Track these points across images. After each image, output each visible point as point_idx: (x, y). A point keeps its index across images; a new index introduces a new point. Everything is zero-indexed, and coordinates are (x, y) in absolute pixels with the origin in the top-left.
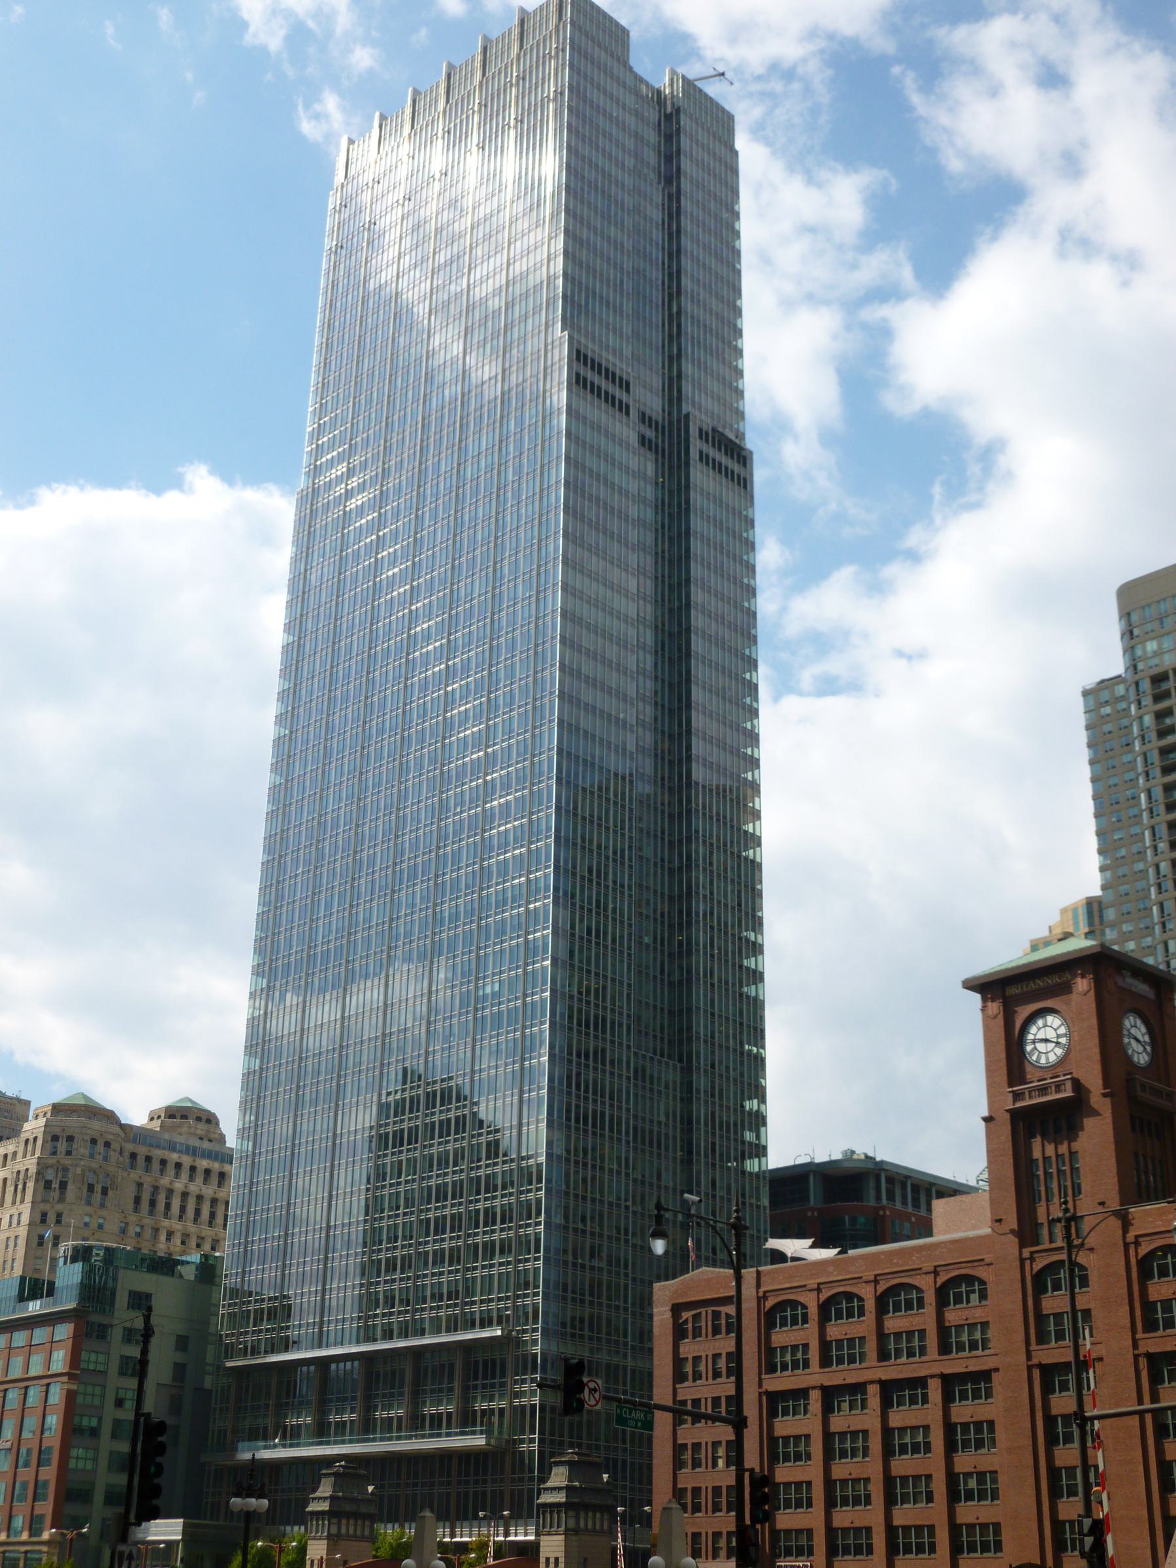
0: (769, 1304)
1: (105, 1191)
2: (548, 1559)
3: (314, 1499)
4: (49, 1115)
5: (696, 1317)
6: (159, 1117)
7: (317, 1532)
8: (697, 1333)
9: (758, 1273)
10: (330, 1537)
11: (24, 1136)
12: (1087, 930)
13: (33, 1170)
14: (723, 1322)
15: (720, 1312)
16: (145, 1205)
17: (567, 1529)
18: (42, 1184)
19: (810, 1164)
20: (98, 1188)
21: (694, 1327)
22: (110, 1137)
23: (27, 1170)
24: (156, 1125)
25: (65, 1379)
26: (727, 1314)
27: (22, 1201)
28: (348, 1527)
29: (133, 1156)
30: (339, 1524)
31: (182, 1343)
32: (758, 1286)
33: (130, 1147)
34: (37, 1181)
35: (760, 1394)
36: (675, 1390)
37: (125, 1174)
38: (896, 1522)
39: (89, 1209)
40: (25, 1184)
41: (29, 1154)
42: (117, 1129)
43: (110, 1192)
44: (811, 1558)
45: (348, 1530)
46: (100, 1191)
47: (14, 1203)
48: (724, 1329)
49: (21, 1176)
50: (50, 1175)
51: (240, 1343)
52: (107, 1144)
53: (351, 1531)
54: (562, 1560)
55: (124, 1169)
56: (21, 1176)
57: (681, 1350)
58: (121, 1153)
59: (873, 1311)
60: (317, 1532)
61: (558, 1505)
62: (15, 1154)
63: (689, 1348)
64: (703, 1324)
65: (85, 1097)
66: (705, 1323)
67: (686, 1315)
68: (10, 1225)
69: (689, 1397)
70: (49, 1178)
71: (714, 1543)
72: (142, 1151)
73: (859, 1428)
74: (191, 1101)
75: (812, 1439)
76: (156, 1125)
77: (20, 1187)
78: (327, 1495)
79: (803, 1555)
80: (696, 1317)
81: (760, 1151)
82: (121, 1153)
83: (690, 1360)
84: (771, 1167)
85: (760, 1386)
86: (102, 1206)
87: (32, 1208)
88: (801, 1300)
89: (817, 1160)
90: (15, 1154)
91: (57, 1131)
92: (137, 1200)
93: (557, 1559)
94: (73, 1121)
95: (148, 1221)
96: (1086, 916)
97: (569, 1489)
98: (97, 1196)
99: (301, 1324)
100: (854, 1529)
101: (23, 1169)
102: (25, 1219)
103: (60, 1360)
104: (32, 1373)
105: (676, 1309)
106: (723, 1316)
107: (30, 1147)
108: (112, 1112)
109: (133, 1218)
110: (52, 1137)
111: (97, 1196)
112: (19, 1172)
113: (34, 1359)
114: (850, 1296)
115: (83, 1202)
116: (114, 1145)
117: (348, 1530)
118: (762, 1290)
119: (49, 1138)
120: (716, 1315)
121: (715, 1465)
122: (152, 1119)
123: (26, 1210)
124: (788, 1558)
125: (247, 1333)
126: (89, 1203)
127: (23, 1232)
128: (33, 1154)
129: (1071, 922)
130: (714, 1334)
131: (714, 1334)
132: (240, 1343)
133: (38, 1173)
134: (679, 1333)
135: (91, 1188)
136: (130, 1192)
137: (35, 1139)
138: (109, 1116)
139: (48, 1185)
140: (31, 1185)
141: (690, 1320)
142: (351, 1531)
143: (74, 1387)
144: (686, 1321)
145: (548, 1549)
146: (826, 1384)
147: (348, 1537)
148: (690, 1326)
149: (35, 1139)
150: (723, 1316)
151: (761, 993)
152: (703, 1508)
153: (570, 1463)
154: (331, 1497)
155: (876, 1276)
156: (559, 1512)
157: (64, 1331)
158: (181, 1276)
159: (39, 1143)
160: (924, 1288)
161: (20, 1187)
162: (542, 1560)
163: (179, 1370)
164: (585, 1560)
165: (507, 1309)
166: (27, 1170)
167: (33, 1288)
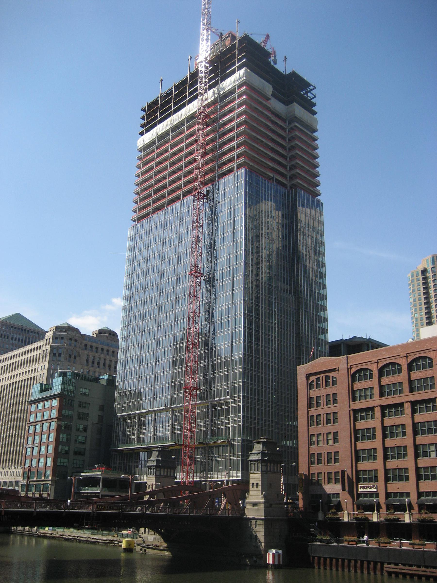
0: (353, 370)
1: (75, 357)
2: (253, 484)
3: (150, 460)
4: (54, 330)
5: (318, 379)
6: (96, 333)
7: (151, 474)
8: (318, 386)
9: (347, 357)
10: (156, 476)
11: (46, 338)
12: (432, 266)
13: (49, 350)
14: (331, 380)
15: (329, 376)
16: (90, 363)
17: (262, 471)
18: (52, 354)
19: (342, 340)
20: (73, 356)
21: (316, 384)
22: (77, 338)
23: (47, 350)
24: (95, 336)
25: (56, 420)
26: (332, 377)
27: (45, 361)
28: (164, 472)
29: (86, 345)
30: (160, 471)
31: (102, 408)
32: (347, 363)
33: (84, 342)
34: (50, 353)
35: (350, 410)
36: (308, 411)
37: (83, 351)
38: (419, 465)
39: (69, 364)
40: (46, 355)
41: (47, 344)
42: (79, 335)
43: (77, 358)
44: (376, 483)
45: (164, 473)
46: (73, 357)
47: (42, 361)
48: (331, 383)
49: (45, 352)
50: (55, 351)
51: (123, 407)
52: (76, 341)
53: (165, 474)
54: (260, 484)
55: (83, 350)
56: (45, 352)
57: (311, 394)
58: (81, 344)
59: (406, 370)
60: (151, 474)
61: (258, 460)
62: (43, 345)
63: (314, 393)
64: (321, 382)
65: (68, 324)
66: (323, 382)
67: (312, 378)
68: (41, 370)
69: (315, 414)
70: (54, 352)
71: (328, 477)
72: (89, 344)
73: (400, 423)
74: (107, 328)
75: (377, 429)
76: (95, 336)
77: (45, 356)
78: (155, 459)
79: (372, 481)
80: (318, 379)
81: (325, 331)
82: (81, 344)
83: (315, 398)
84: (330, 341)
85: (350, 408)
86: (74, 363)
87: (49, 363)
88: (369, 368)
89: (344, 339)
90: (43, 345)
91: (58, 336)
92: (87, 361)
93: (257, 484)
94: (64, 333)
95: (91, 368)
96: (432, 262)
97: (263, 454)
98: (73, 359)
99: (146, 401)
100: (398, 469)
101: (45, 349)
102: (46, 367)
103: (54, 413)
104: (45, 418)
105: (308, 376)
106: (331, 378)
107: (48, 342)
108: (78, 329)
109: (86, 367)
110: (56, 337)
111: (73, 359)
112: (44, 351)
113: (45, 413)
114: (393, 364)
115: (67, 361)
116: (79, 341)
117: (164, 473)
118: (349, 365)
119: (55, 338)
120: (327, 378)
121: (328, 443)
122: (93, 334)
123: (46, 363)
124: (364, 483)
125: (125, 403)
126: (70, 362)
127: (45, 371)
128: (49, 344)
129: (426, 264)
130: (326, 386)
131: (326, 386)
132: (123, 407)
133: (51, 351)
134: (310, 386)
135: (70, 356)
136: (85, 358)
137: (50, 338)
138: (77, 331)
139: (54, 355)
140: (48, 355)
141: (315, 381)
142: (165, 474)
143: (60, 423)
144: (313, 381)
145: (253, 480)
146: (382, 404)
147: (164, 476)
148: (315, 383)
149: (50, 338)
150: (331, 378)
151: (324, 271)
152: (323, 462)
153: (263, 443)
154: (157, 460)
155: (407, 354)
156: (258, 464)
157: (55, 402)
158: (100, 383)
159: (51, 340)
160: (432, 358)
161: (45, 356)
162: (251, 485)
163: (101, 418)
164: (270, 484)
165: (228, 389)
166: (47, 350)
167: (45, 388)
